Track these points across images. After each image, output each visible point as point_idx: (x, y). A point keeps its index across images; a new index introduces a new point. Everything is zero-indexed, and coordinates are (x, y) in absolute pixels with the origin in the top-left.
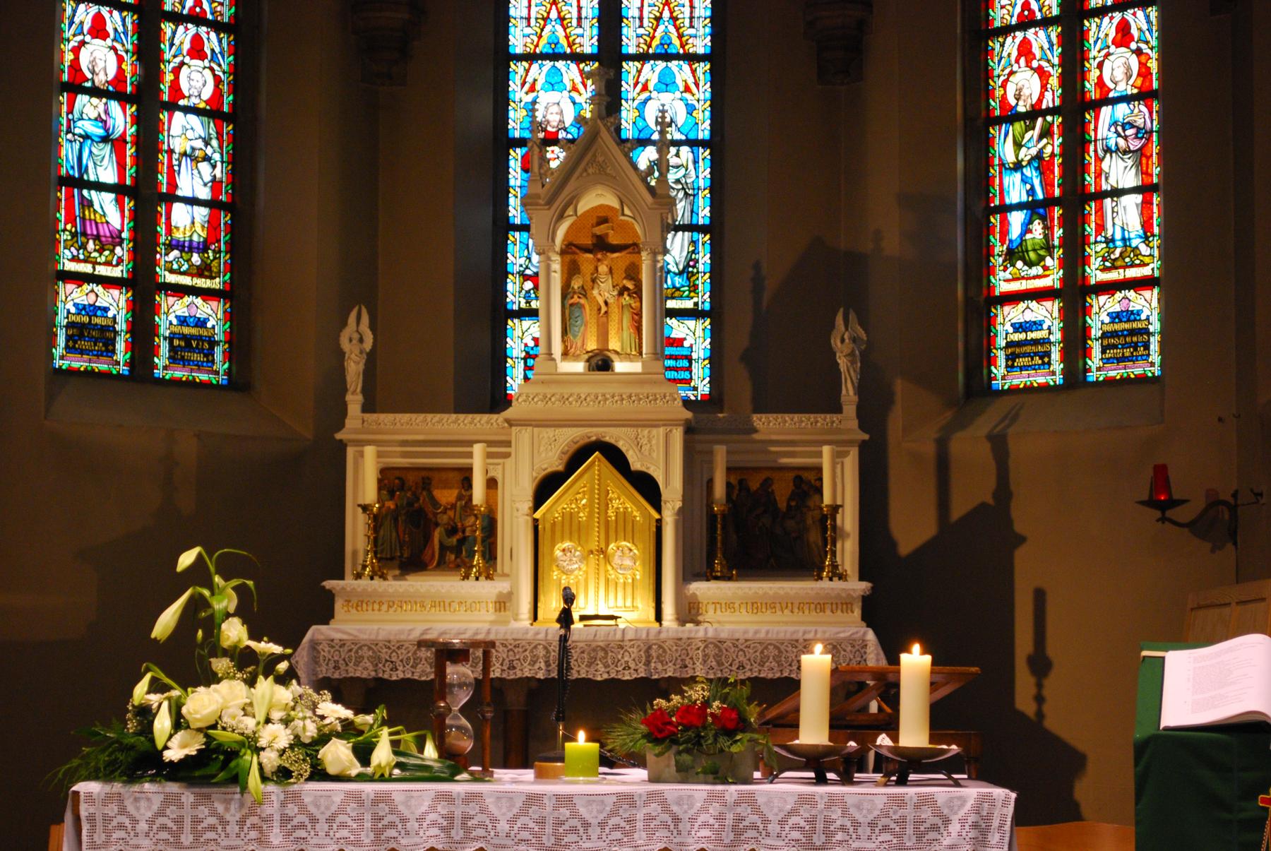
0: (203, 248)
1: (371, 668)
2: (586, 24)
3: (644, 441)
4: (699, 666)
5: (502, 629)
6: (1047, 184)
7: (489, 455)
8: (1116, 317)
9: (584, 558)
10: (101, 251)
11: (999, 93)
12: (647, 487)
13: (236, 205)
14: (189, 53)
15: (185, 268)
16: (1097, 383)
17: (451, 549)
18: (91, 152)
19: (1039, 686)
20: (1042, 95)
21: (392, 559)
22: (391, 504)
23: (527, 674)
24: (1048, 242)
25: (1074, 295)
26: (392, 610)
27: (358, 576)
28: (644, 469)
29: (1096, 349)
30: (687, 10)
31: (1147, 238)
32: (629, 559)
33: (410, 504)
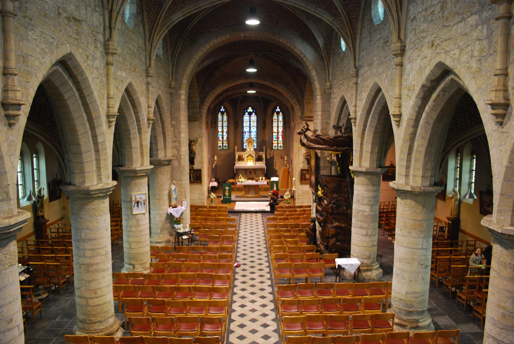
13: (228, 138)
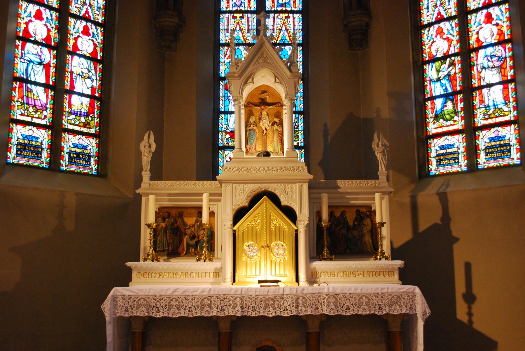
0: (87, 115)
1: (145, 311)
2: (251, 32)
3: (289, 190)
4: (325, 308)
5: (217, 287)
6: (453, 86)
7: (211, 200)
8: (492, 139)
9: (259, 250)
10: (36, 112)
11: (427, 51)
12: (290, 213)
13: (102, 98)
14: (82, 32)
15: (77, 123)
16: (484, 169)
17: (192, 246)
18: (32, 68)
19: (470, 308)
20: (449, 49)
21: (164, 251)
22: (163, 225)
23: (231, 314)
24: (455, 110)
25: (470, 131)
26: (161, 277)
27: (145, 260)
28: (289, 205)
29: (483, 155)
30: (292, 26)
31: (506, 104)
32: (282, 250)
33: (173, 224)
